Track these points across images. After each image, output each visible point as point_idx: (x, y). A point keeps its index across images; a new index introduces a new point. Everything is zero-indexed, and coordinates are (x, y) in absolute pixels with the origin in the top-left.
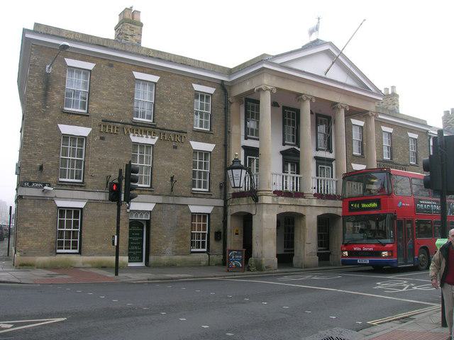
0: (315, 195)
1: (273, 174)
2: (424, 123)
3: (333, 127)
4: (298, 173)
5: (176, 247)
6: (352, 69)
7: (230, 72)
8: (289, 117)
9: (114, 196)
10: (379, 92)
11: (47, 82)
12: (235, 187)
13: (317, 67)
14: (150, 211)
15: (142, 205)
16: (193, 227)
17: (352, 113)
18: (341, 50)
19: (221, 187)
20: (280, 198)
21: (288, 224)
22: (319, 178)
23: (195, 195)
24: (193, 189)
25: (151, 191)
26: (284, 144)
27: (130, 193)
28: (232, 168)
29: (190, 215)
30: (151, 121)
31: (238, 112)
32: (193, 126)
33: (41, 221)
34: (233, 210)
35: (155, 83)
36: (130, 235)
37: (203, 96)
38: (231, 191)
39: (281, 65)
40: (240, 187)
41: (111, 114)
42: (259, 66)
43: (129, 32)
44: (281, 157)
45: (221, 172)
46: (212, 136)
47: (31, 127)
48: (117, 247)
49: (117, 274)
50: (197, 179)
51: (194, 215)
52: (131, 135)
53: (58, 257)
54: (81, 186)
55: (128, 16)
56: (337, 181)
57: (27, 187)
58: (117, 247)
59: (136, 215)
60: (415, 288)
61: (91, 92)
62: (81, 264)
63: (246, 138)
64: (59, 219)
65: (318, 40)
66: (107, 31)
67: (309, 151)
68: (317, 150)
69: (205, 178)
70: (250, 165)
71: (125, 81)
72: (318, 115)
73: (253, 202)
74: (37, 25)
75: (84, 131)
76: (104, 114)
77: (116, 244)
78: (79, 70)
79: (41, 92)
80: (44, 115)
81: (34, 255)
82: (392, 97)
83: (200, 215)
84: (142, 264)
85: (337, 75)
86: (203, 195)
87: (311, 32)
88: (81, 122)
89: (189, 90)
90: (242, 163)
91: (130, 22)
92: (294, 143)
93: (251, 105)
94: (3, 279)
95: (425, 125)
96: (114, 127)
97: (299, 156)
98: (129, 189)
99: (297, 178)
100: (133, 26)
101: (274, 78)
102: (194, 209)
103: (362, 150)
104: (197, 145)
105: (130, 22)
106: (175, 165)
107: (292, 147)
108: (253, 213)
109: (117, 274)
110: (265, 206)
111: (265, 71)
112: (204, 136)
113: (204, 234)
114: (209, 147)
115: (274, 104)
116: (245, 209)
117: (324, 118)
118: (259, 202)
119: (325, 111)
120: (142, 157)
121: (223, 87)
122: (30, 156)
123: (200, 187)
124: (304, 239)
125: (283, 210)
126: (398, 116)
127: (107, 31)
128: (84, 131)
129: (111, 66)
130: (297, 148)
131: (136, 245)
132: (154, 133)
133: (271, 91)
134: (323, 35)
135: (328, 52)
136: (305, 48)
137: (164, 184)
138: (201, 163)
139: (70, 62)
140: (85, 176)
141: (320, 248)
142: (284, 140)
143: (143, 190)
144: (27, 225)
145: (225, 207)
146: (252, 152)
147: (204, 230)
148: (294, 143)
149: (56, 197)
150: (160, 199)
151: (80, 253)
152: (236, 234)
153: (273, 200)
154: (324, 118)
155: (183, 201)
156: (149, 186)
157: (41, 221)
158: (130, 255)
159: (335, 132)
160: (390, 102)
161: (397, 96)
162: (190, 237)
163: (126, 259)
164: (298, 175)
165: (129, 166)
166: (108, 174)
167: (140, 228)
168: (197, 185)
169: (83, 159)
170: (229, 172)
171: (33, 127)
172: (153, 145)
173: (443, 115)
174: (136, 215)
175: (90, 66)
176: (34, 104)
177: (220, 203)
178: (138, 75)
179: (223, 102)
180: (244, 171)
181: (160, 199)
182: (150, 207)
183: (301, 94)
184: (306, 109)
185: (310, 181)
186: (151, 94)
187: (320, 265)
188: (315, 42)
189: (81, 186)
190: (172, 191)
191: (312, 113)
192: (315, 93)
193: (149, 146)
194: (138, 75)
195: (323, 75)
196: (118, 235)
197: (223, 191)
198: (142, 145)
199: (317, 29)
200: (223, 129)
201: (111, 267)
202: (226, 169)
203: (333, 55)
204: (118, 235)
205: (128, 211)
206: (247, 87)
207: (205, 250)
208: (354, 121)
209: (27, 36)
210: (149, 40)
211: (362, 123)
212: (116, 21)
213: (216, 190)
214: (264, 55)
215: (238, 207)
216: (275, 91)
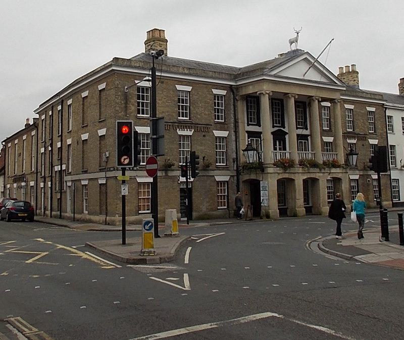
3: (308, 110)
6: (324, 71)
11: (127, 99)
13: (297, 71)
21: (284, 186)
24: (217, 164)
26: (274, 127)
31: (242, 108)
35: (189, 92)
39: (275, 76)
53: (140, 216)
55: (157, 35)
63: (248, 125)
71: (172, 92)
83: (221, 182)
85: (313, 76)
86: (223, 168)
87: (291, 43)
91: (156, 39)
93: (253, 101)
99: (283, 153)
100: (161, 43)
102: (218, 179)
103: (330, 126)
104: (217, 133)
105: (156, 39)
108: (261, 179)
110: (269, 174)
112: (222, 126)
114: (224, 134)
116: (253, 177)
124: (295, 197)
125: (280, 177)
130: (282, 129)
132: (191, 127)
134: (301, 45)
141: (280, 205)
142: (273, 124)
149: (137, 176)
152: (246, 195)
154: (303, 105)
155: (212, 173)
159: (310, 117)
160: (351, 78)
164: (285, 151)
176: (120, 114)
180: (255, 152)
187: (306, 215)
192: (298, 91)
193: (188, 136)
195: (302, 78)
198: (184, 136)
206: (250, 90)
207: (226, 207)
210: (173, 52)
216: (271, 94)
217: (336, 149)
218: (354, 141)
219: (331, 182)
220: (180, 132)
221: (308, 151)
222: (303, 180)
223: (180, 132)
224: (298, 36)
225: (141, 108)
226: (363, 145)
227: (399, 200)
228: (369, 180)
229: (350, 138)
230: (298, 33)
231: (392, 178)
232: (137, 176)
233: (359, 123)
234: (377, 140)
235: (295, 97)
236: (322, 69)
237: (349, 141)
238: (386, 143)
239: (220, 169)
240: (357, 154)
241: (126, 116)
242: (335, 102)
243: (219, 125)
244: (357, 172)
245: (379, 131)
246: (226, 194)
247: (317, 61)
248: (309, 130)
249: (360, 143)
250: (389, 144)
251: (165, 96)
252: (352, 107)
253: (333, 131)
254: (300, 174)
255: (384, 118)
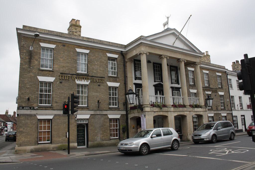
0: (172, 106)
1: (149, 95)
2: (224, 68)
4: (163, 95)
5: (103, 136)
6: (186, 42)
7: (126, 47)
8: (157, 71)
9: (66, 111)
10: (200, 52)
12: (130, 104)
13: (169, 41)
14: (88, 119)
15: (82, 116)
16: (110, 126)
17: (188, 64)
18: (180, 32)
19: (124, 105)
20: (154, 108)
22: (174, 97)
23: (111, 109)
24: (110, 106)
25: (87, 108)
26: (155, 81)
27: (73, 109)
28: (128, 94)
29: (109, 120)
30: (86, 73)
31: (130, 68)
32: (108, 74)
33: (29, 127)
34: (130, 116)
35: (88, 54)
36: (78, 132)
37: (113, 59)
38: (129, 106)
39: (151, 41)
40: (133, 104)
41: (66, 70)
42: (140, 42)
43: (74, 30)
44: (154, 88)
45: (124, 97)
46: (118, 79)
47: (23, 78)
48: (69, 138)
49: (69, 153)
50: (112, 101)
51: (111, 120)
52: (76, 80)
54: (51, 108)
55: (74, 23)
56: (183, 98)
57: (21, 109)
58: (69, 138)
59: (81, 121)
60: (233, 152)
61: (54, 59)
62: (52, 149)
63: (135, 79)
64: (39, 125)
65: (168, 28)
66: (64, 29)
67: (167, 84)
68: (172, 83)
69: (116, 100)
70: (138, 93)
72: (171, 66)
73: (141, 111)
74: (24, 26)
75: (51, 79)
76: (61, 70)
77: (68, 137)
78: (47, 49)
79: (28, 60)
80: (29, 72)
81: (26, 145)
82: (208, 56)
83: (114, 119)
84: (85, 147)
87: (164, 25)
88: (49, 74)
89: (105, 57)
90: (134, 91)
91: (75, 25)
92: (160, 81)
93: (137, 62)
94: (2, 161)
95: (225, 69)
96: (67, 77)
97: (163, 87)
98: (73, 107)
99: (162, 97)
100: (76, 27)
101: (147, 48)
102: (110, 117)
103: (194, 81)
104: (110, 84)
105: (75, 25)
106: (100, 94)
107: (159, 83)
109: (69, 153)
110: (147, 113)
111: (142, 44)
112: (114, 79)
113: (117, 129)
114: (117, 85)
115: (149, 62)
117: (174, 69)
118: (144, 111)
119: (175, 64)
120: (82, 91)
121: (122, 54)
122: (22, 93)
123: (113, 105)
125: (156, 114)
126: (210, 65)
127: (64, 29)
128: (51, 79)
129: (64, 46)
130: (161, 83)
131: (82, 137)
132: (88, 78)
133: (146, 54)
134: (171, 26)
135: (173, 34)
136: (163, 32)
137: (94, 104)
138: (113, 93)
139: (43, 45)
140: (53, 102)
142: (155, 79)
143: (83, 108)
144: (21, 129)
145: (127, 115)
146: (139, 86)
147: (117, 127)
148: (160, 81)
149: (37, 114)
150: (92, 112)
151: (51, 143)
153: (151, 109)
154: (174, 69)
155: (105, 113)
156: (87, 106)
157: (29, 127)
158: (78, 143)
159: (180, 76)
160: (206, 59)
161: (209, 56)
162: (109, 131)
163: (76, 144)
165: (73, 95)
166: (65, 101)
167: (82, 128)
168: (112, 104)
169: (51, 94)
170: (127, 96)
171: (24, 78)
172: (88, 85)
173: (232, 64)
174: (81, 121)
175: (53, 46)
177: (124, 113)
178: (78, 50)
179: (123, 61)
181: (92, 112)
182: (87, 117)
183: (180, 59)
184: (165, 63)
185: (169, 99)
186: (85, 60)
188: (167, 29)
189: (50, 108)
190: (99, 107)
191: (168, 65)
193: (85, 86)
194: (78, 50)
196: (69, 131)
197: (125, 106)
198: (82, 86)
199: (167, 23)
200: (123, 75)
201: (71, 149)
202: (126, 94)
203: (176, 35)
204: (69, 131)
205: (76, 119)
206: (134, 53)
207: (118, 137)
208: (189, 69)
209: (19, 32)
210: (85, 33)
211: (193, 69)
212: (68, 26)
213: (121, 106)
214: (142, 36)
215: (133, 114)
216: (148, 54)
217: (198, 96)
218: (210, 93)
219: (196, 118)
220: (78, 82)
221: (180, 96)
222: (175, 116)
223: (78, 82)
224: (168, 20)
225: (111, 92)
226: (215, 95)
227: (238, 128)
228: (220, 117)
229: (208, 90)
230: (168, 18)
231: (233, 115)
232: (37, 114)
233: (212, 82)
234: (224, 93)
235: (167, 58)
236: (184, 40)
237: (207, 93)
238: (229, 95)
239: (113, 110)
240: (212, 99)
241: (30, 68)
242: (196, 64)
243: (111, 79)
244: (213, 112)
245: (224, 87)
246: (118, 128)
247: (180, 34)
248: (180, 84)
249: (214, 94)
250: (230, 95)
251: (66, 55)
252: (207, 72)
253: (196, 86)
254: (172, 112)
255: (227, 80)
